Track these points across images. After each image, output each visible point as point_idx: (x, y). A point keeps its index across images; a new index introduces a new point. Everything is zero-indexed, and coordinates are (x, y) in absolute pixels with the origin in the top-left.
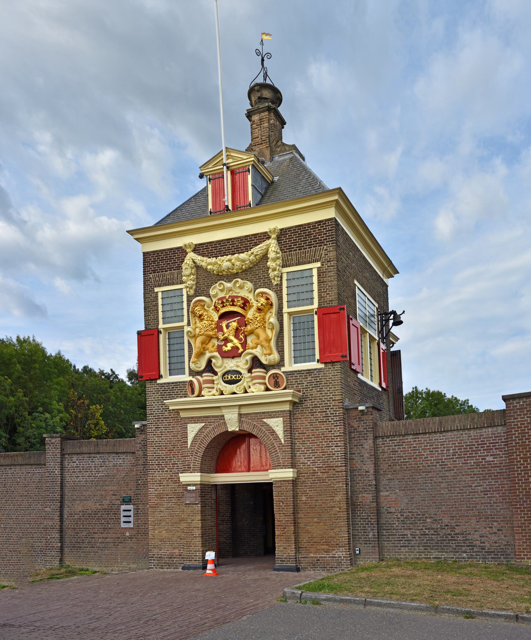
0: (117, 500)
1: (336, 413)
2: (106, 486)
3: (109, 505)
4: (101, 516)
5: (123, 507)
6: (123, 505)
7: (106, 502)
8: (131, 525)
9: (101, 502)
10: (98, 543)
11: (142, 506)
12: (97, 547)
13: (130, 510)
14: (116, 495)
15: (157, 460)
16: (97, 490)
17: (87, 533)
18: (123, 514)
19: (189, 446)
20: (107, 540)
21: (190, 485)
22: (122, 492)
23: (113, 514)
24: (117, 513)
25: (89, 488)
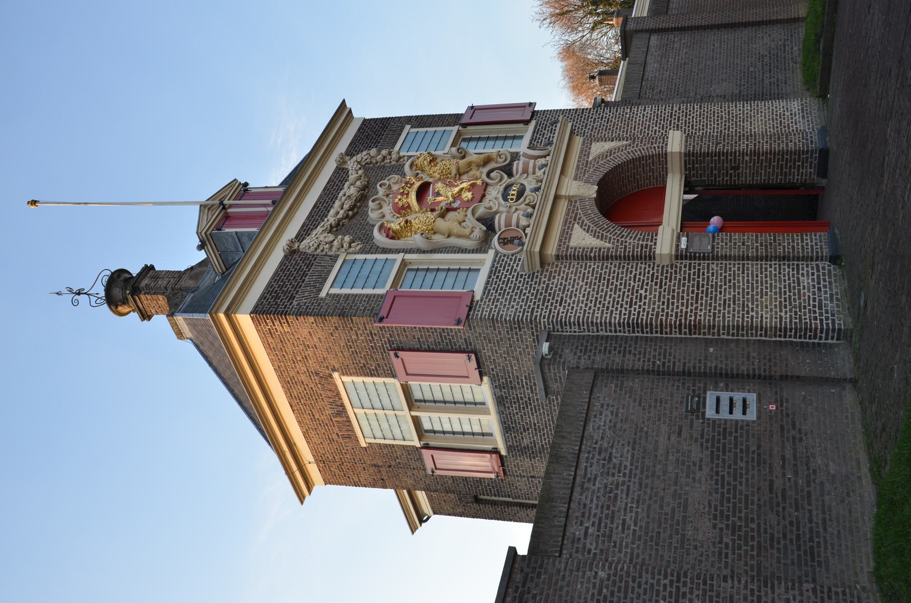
0: (691, 427)
1: (515, 328)
2: (656, 449)
3: (702, 445)
4: (729, 467)
5: (710, 413)
6: (704, 413)
7: (696, 453)
8: (752, 398)
9: (694, 464)
10: (796, 483)
11: (711, 362)
12: (808, 484)
13: (718, 399)
14: (680, 428)
15: (622, 305)
16: (665, 473)
17: (772, 509)
18: (724, 414)
19: (607, 245)
20: (788, 455)
21: (678, 246)
22: (675, 414)
23: (725, 438)
24: (723, 429)
25: (656, 494)
